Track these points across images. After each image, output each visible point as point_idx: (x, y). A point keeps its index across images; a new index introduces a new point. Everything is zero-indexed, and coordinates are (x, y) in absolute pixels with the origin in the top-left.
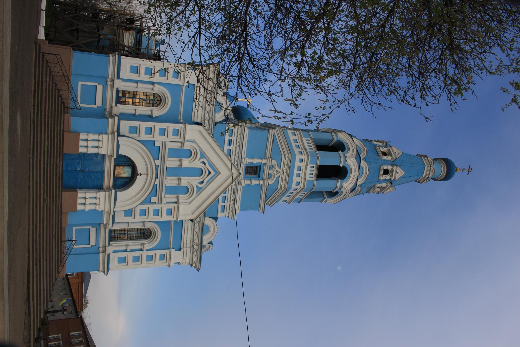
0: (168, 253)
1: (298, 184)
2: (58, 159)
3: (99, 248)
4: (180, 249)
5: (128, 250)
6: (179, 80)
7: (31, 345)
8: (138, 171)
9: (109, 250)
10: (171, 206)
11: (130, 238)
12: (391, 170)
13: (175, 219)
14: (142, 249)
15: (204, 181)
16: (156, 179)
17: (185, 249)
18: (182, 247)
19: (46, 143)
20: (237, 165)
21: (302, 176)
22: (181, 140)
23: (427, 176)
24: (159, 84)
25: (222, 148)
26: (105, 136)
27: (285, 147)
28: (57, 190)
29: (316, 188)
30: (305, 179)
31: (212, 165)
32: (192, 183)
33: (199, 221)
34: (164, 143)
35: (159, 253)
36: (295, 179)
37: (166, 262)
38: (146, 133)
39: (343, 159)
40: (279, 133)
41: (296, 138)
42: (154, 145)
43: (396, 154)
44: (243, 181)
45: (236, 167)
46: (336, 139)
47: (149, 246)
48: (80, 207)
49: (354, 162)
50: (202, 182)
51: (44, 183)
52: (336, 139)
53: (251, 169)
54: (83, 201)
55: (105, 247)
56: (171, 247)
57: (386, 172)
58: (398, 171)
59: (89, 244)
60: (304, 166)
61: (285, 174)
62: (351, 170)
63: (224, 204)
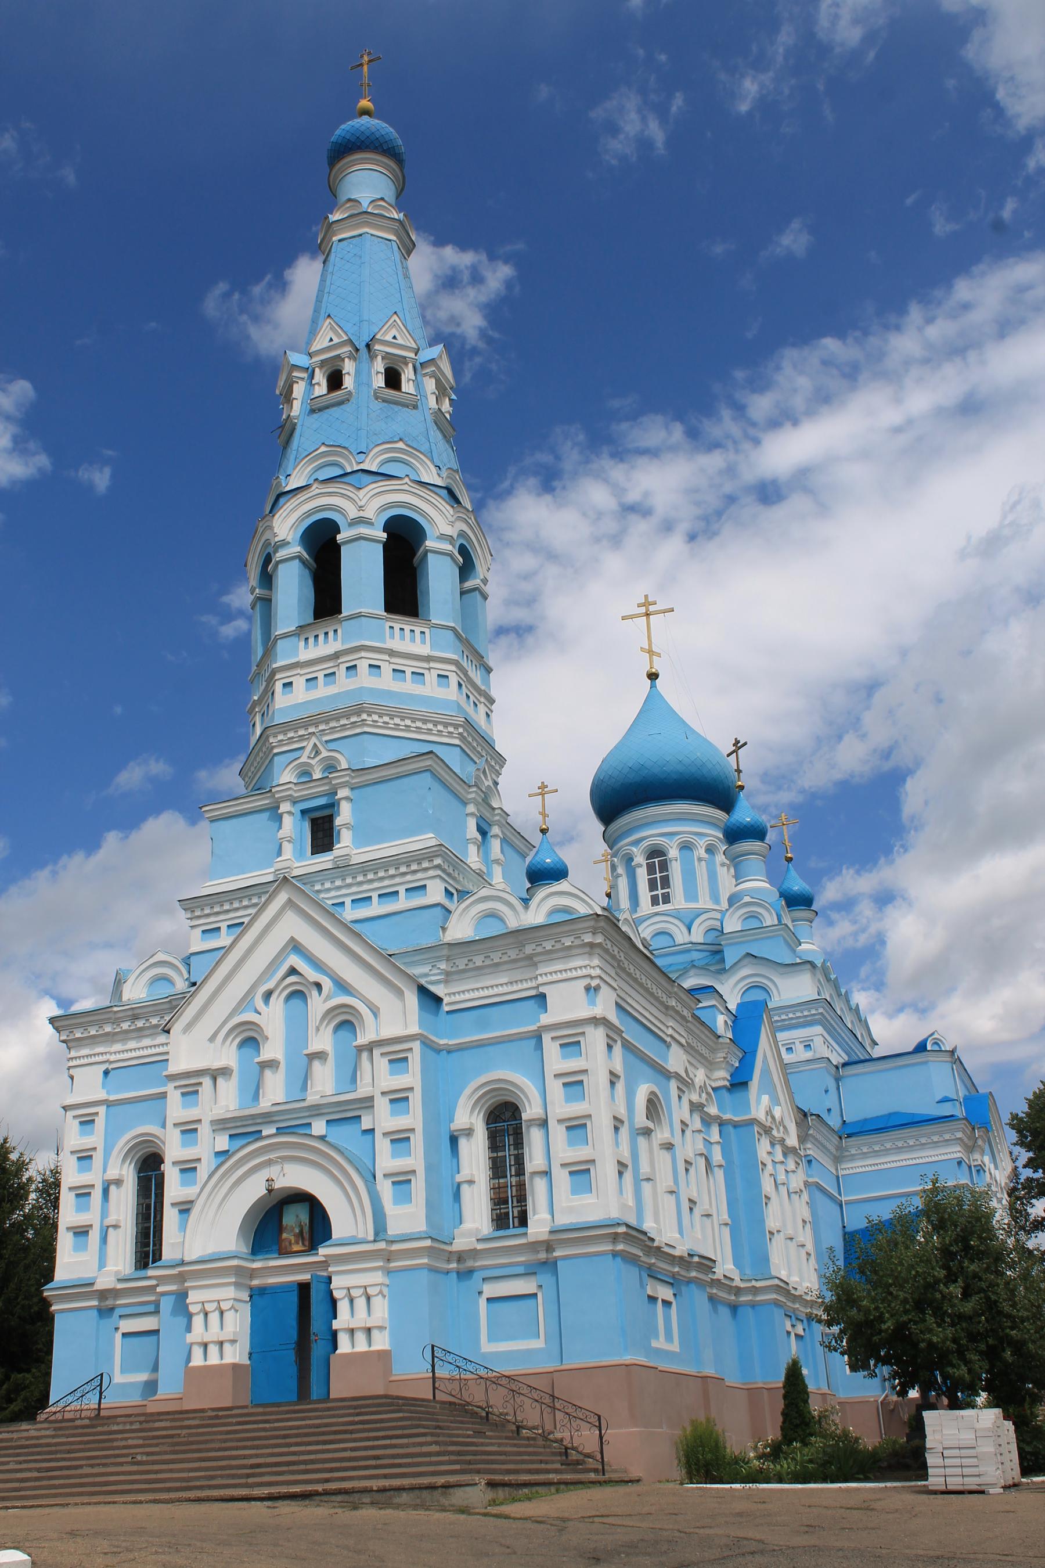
2: (99, 1429)
6: (409, 1055)
18: (533, 993)
26: (193, 1297)
29: (454, 622)
33: (448, 959)
34: (220, 1125)
39: (364, 530)
41: (299, 683)
43: (336, 340)
46: (299, 549)
48: (381, 1342)
49: (284, 514)
52: (297, 549)
54: (213, 1350)
55: (534, 1246)
57: (335, 381)
58: (326, 344)
62: (301, 519)
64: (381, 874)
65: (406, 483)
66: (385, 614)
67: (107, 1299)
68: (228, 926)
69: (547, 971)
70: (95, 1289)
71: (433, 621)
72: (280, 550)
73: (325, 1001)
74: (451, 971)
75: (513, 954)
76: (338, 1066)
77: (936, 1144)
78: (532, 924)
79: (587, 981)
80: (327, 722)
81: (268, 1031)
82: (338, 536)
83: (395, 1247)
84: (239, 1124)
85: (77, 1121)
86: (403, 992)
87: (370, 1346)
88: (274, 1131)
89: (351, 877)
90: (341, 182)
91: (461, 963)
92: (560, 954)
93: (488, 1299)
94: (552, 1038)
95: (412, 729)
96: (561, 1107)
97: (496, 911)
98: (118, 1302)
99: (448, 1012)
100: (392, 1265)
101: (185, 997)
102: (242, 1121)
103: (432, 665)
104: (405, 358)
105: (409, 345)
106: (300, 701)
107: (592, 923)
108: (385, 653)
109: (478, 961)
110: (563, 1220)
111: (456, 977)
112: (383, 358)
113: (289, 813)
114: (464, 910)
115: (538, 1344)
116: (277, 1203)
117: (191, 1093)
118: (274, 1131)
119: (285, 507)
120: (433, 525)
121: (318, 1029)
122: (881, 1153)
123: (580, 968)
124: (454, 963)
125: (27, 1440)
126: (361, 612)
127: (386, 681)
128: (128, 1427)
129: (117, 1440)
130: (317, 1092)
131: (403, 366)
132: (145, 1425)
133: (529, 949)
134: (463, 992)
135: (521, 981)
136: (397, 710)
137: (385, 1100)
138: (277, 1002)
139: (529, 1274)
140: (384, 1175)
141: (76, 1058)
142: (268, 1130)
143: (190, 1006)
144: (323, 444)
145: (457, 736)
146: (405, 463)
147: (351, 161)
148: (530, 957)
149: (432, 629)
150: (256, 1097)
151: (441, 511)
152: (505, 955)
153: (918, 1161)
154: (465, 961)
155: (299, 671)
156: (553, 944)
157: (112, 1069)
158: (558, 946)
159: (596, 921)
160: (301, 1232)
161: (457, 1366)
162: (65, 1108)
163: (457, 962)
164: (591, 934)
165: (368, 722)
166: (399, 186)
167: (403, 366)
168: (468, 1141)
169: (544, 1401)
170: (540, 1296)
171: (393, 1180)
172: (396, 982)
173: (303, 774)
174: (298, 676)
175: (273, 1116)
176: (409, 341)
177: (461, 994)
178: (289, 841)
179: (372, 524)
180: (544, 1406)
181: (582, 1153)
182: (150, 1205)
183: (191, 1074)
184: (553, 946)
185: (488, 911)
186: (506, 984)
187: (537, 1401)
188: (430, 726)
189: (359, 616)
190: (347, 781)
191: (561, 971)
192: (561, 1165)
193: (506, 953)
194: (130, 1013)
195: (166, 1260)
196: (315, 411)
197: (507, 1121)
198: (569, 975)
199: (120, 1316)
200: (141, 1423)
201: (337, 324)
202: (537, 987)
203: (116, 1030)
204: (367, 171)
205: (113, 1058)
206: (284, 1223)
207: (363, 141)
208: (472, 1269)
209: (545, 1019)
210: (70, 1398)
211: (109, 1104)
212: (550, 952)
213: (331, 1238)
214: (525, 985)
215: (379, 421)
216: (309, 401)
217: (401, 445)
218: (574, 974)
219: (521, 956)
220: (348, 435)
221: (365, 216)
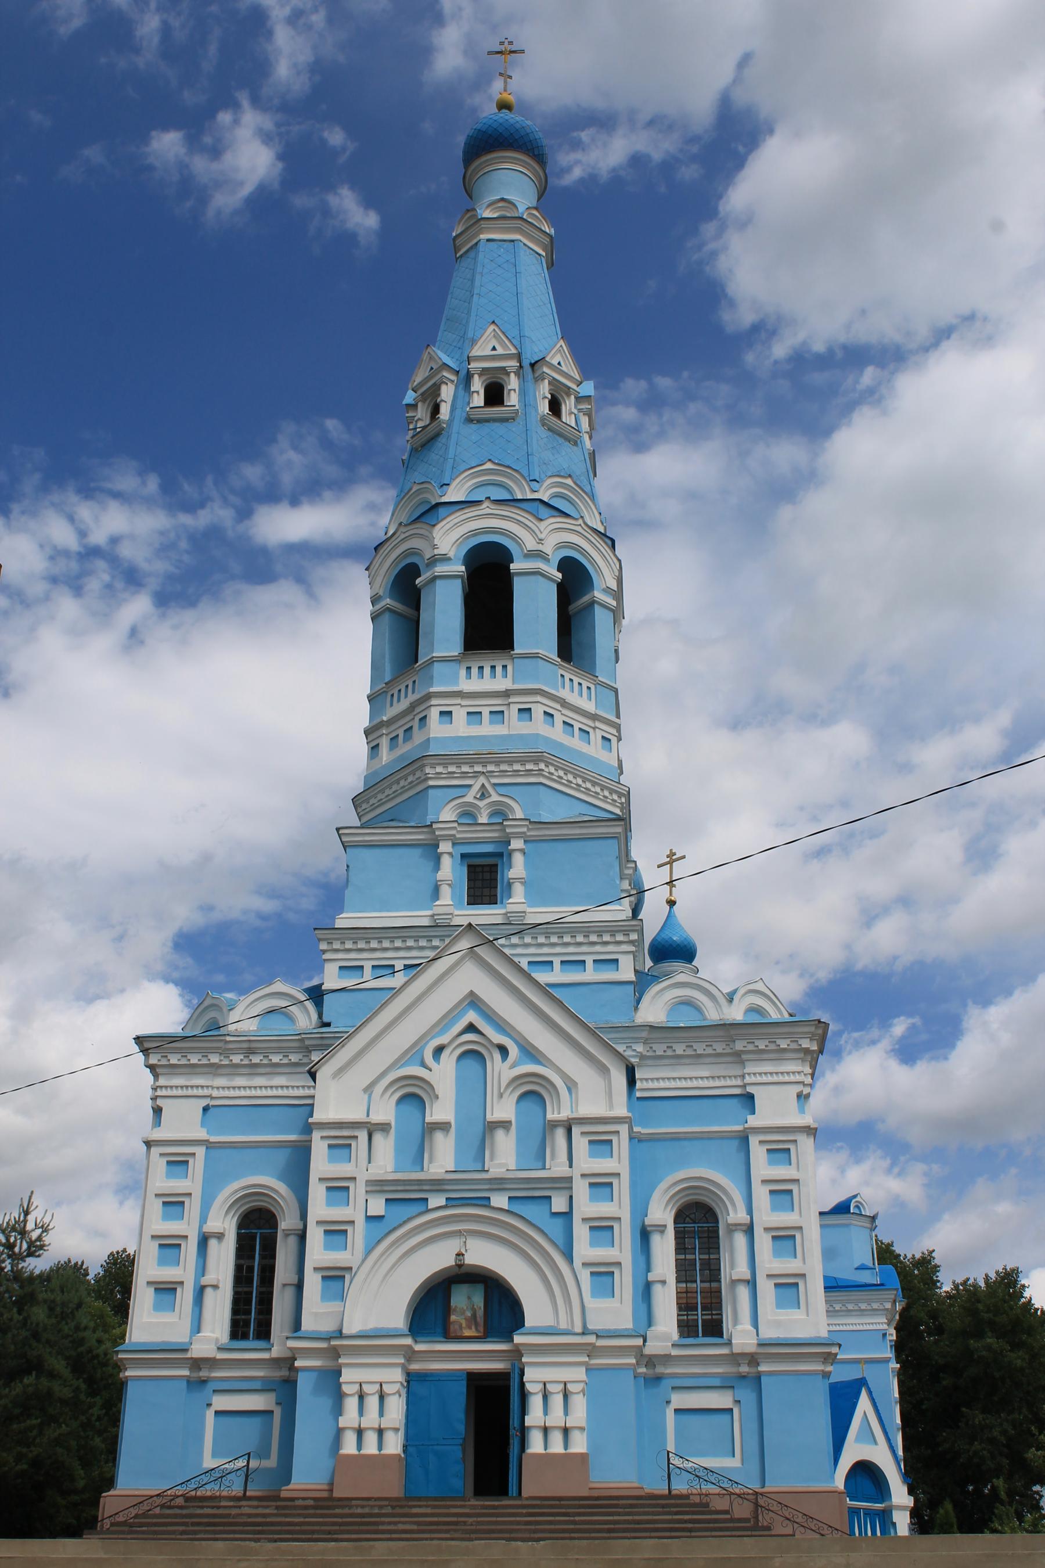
0: (763, 1138)
2: (337, 1511)
4: (751, 1097)
8: (451, 1264)
10: (581, 1144)
11: (713, 1272)
14: (744, 1228)
15: (496, 1042)
17: (748, 1080)
18: (737, 1091)
20: (442, 938)
22: (363, 1136)
24: (203, 1219)
26: (347, 1375)
32: (503, 1085)
33: (646, 1042)
34: (377, 1186)
35: (762, 1166)
39: (541, 565)
40: (372, 801)
41: (460, 715)
42: (382, 1217)
43: (500, 351)
46: (388, 601)
48: (579, 1445)
49: (448, 526)
50: (503, 1050)
53: (479, 884)
54: (371, 1438)
55: (735, 1358)
57: (495, 395)
58: (488, 352)
59: (732, 1409)
62: (476, 533)
63: (589, 964)
64: (567, 939)
65: (580, 525)
66: (559, 660)
67: (200, 1369)
68: (373, 967)
69: (756, 1071)
70: (189, 1355)
71: (600, 678)
72: (438, 564)
73: (513, 1066)
74: (645, 1055)
75: (719, 1048)
76: (520, 1141)
77: (862, 1312)
78: (734, 1020)
79: (799, 1088)
80: (497, 763)
81: (439, 1090)
82: (511, 565)
83: (601, 1343)
84: (400, 1188)
85: (164, 1160)
86: (608, 1070)
87: (545, 1450)
88: (443, 1202)
89: (530, 936)
90: (485, 176)
91: (660, 1049)
92: (772, 1056)
93: (675, 1410)
94: (760, 1142)
95: (582, 789)
96: (766, 1215)
97: (693, 999)
98: (214, 1374)
99: (638, 1098)
100: (593, 1362)
101: (342, 1037)
102: (405, 1185)
103: (598, 724)
104: (569, 388)
105: (572, 374)
106: (460, 735)
107: (812, 1029)
108: (558, 702)
109: (680, 1049)
110: (768, 1333)
111: (649, 1062)
112: (550, 383)
113: (450, 854)
114: (658, 993)
115: (735, 1462)
116: (444, 1280)
117: (341, 1147)
118: (443, 1202)
119: (449, 519)
120: (599, 575)
121: (501, 1096)
122: (854, 1313)
123: (793, 1073)
124: (651, 1048)
125: (250, 1518)
126: (538, 653)
127: (556, 733)
128: (376, 1511)
129: (383, 1523)
130: (500, 1165)
131: (565, 397)
132: (398, 1510)
133: (739, 1046)
134: (658, 1079)
135: (724, 1077)
136: (572, 766)
137: (585, 1183)
138: (449, 1059)
139: (726, 1385)
140: (583, 1264)
141: (166, 1087)
142: (436, 1201)
143: (343, 1049)
144: (490, 460)
145: (619, 805)
146: (570, 502)
147: (487, 160)
148: (738, 1054)
149: (598, 686)
150: (419, 1159)
151: (610, 565)
152: (710, 1048)
153: (841, 1328)
154: (664, 1047)
155: (458, 701)
157: (213, 1106)
158: (772, 1047)
159: (817, 1027)
160: (474, 1315)
161: (697, 1476)
162: (148, 1144)
163: (655, 1047)
164: (809, 1039)
165: (544, 773)
166: (540, 185)
167: (565, 397)
168: (662, 1238)
169: (797, 1520)
170: (736, 1412)
171: (591, 1270)
172: (601, 1058)
173: (463, 815)
174: (459, 706)
175: (444, 1184)
176: (573, 370)
177: (195, 1088)
178: (449, 885)
179: (548, 560)
180: (796, 1525)
181: (792, 1265)
182: (253, 1267)
183: (344, 1125)
184: (766, 1046)
185: (683, 998)
186: (707, 1078)
187: (788, 1519)
188: (598, 789)
189: (535, 656)
190: (524, 833)
191: (771, 1073)
192: (767, 1275)
193: (186, 1056)
194: (245, 1045)
195: (307, 1331)
196: (472, 421)
197: (698, 1223)
198: (781, 1078)
199: (214, 1391)
200: (393, 1507)
201: (503, 333)
202: (744, 1086)
203: (223, 1063)
204: (517, 172)
205: (215, 1093)
206: (453, 1303)
207: (506, 138)
208: (660, 1376)
209: (753, 1121)
210: (205, 1479)
211: (209, 1145)
212: (762, 1051)
214: (729, 1082)
215: (546, 450)
216: (468, 409)
217: (569, 481)
218: (786, 1078)
219: (728, 1051)
220: (516, 457)
221: (520, 222)
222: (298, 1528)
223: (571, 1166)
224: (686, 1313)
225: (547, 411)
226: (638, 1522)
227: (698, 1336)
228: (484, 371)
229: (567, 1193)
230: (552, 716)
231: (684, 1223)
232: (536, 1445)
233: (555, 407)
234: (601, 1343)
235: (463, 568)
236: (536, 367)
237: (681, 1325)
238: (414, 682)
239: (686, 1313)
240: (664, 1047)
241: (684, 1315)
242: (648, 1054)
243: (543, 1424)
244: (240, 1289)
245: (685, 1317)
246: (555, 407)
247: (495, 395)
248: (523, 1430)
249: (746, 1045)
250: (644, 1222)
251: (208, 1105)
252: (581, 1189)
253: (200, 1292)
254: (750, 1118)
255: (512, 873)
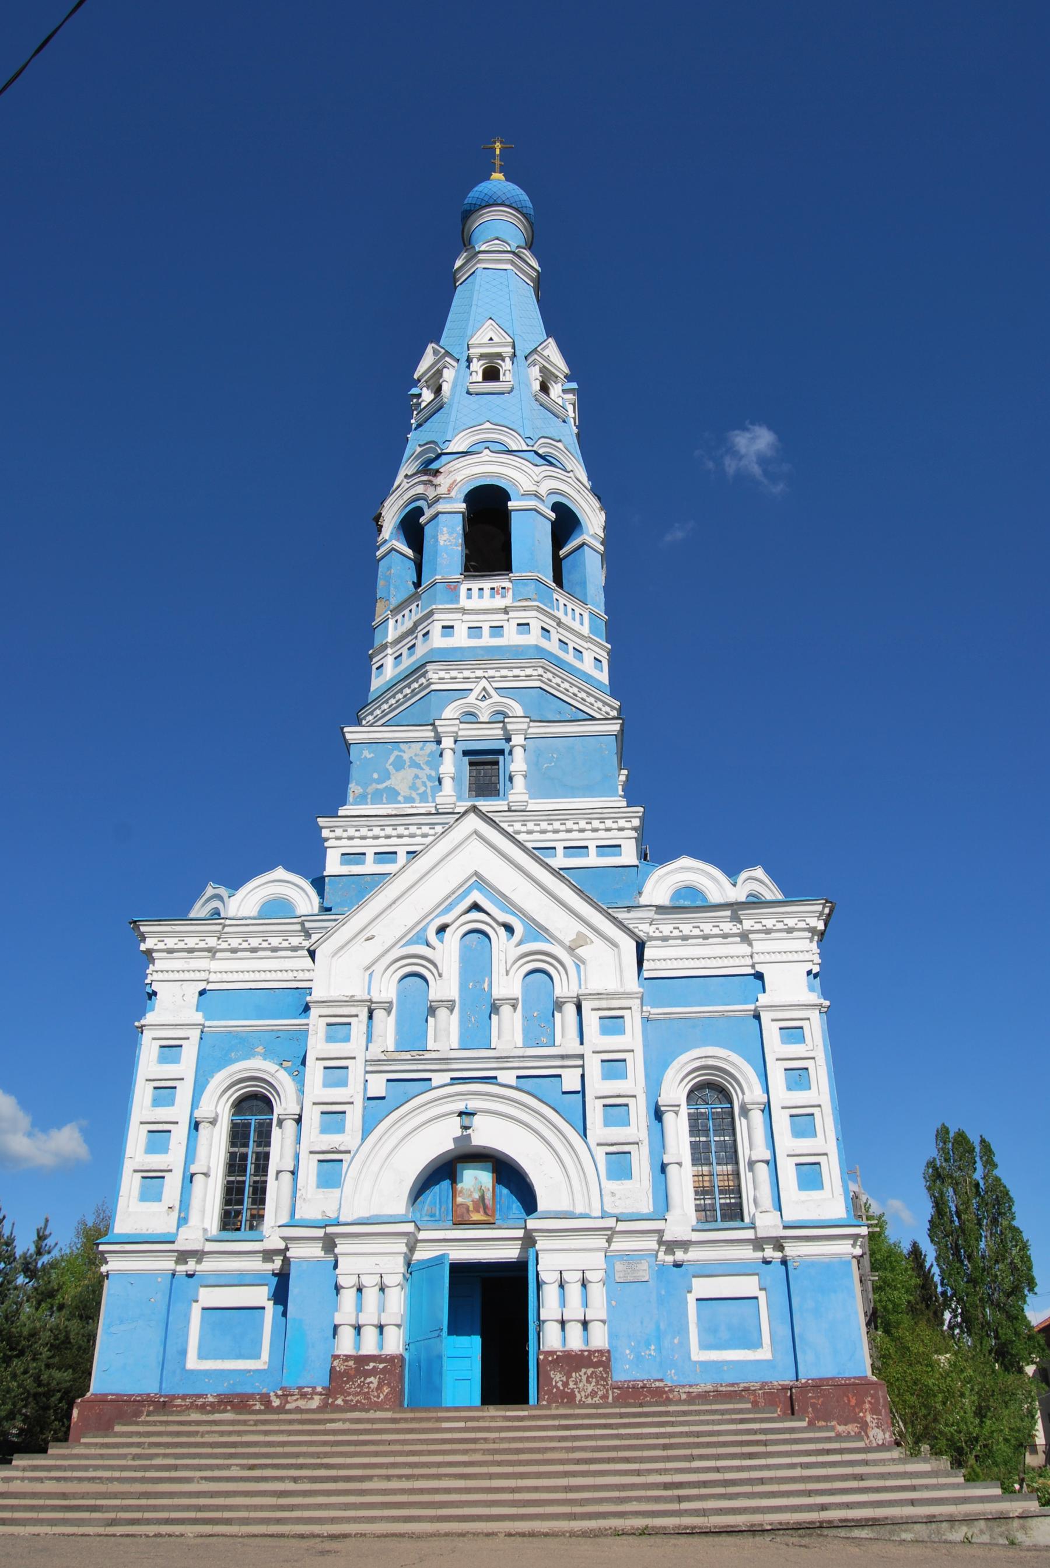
1: (524, 626)
3: (766, 1262)
4: (759, 976)
5: (768, 1156)
7: (1020, 1510)
9: (768, 1224)
12: (482, 362)
13: (635, 1003)
16: (500, 1080)
17: (756, 959)
19: (235, 1472)
21: (498, 619)
23: (510, 256)
24: (195, 1104)
25: (378, 880)
27: (408, 686)
28: (445, 1425)
30: (506, 610)
31: (447, 904)
32: (510, 962)
35: (774, 1044)
36: (512, 637)
37: (808, 1019)
38: (341, 1129)
44: (511, 798)
45: (447, 826)
47: (747, 1079)
48: (599, 1338)
50: (509, 929)
51: (370, 1478)
54: (370, 1335)
55: (758, 1243)
56: (752, 1007)
57: (491, 374)
58: (546, 355)
60: (466, 617)
61: (491, 673)
63: (592, 850)
66: (554, 585)
73: (519, 944)
74: (652, 937)
81: (444, 968)
83: (621, 1226)
110: (789, 1216)
124: (657, 929)
125: (222, 1436)
126: (435, 580)
138: (453, 937)
156: (775, 923)
166: (528, 236)
197: (711, 1104)
213: (537, 1211)
214: (737, 962)
222: (279, 1450)
223: (582, 1043)
224: (702, 1197)
225: (538, 387)
226: (698, 1434)
227: (716, 1221)
228: (482, 356)
229: (580, 1071)
230: (548, 631)
231: (697, 1104)
232: (552, 1339)
233: (544, 388)
234: (621, 1226)
235: (464, 505)
236: (528, 358)
237: (699, 1209)
238: (418, 606)
239: (702, 1197)
240: (671, 927)
241: (701, 1199)
242: (654, 935)
243: (560, 1318)
244: (232, 1179)
245: (702, 1202)
246: (544, 388)
247: (491, 374)
248: (540, 1323)
249: (753, 924)
250: (657, 1101)
251: (205, 989)
252: (594, 1066)
253: (190, 1178)
254: (761, 996)
255: (513, 767)
